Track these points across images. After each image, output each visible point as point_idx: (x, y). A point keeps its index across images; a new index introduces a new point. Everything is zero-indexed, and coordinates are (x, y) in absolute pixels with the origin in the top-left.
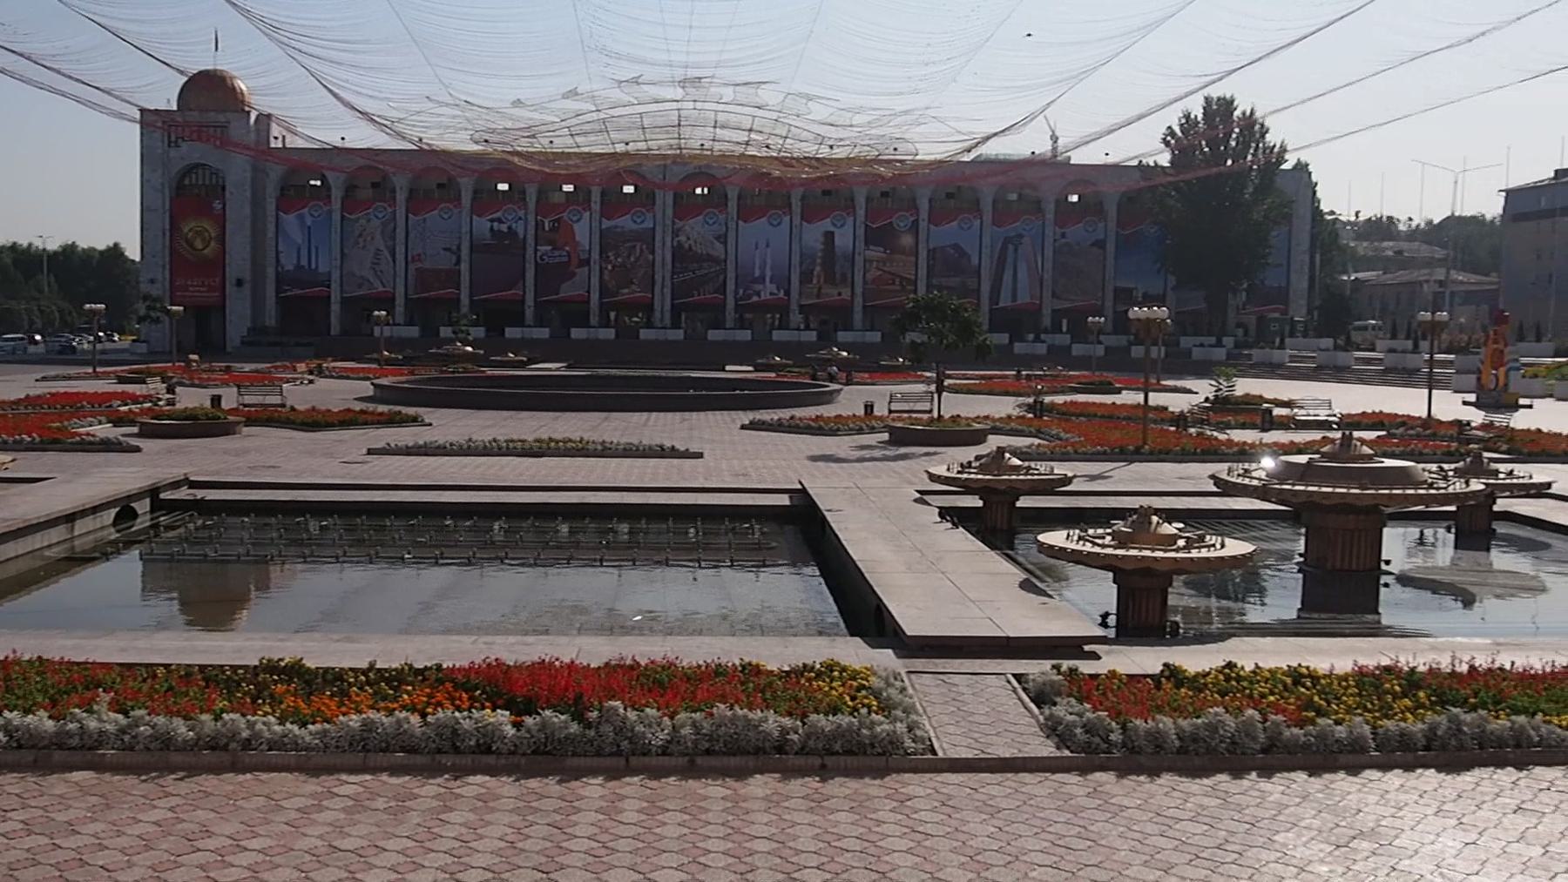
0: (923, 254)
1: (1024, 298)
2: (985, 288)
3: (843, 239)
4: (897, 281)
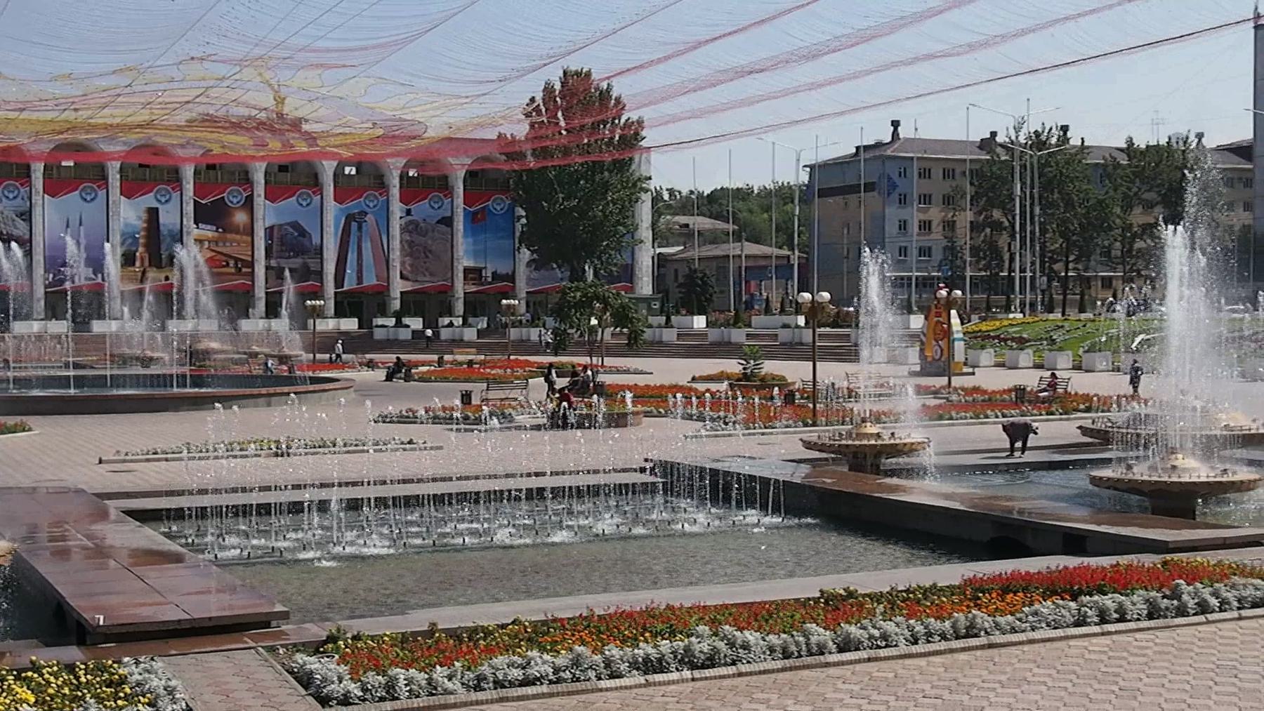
0: (260, 234)
1: (370, 280)
2: (330, 268)
3: (168, 218)
4: (232, 263)
